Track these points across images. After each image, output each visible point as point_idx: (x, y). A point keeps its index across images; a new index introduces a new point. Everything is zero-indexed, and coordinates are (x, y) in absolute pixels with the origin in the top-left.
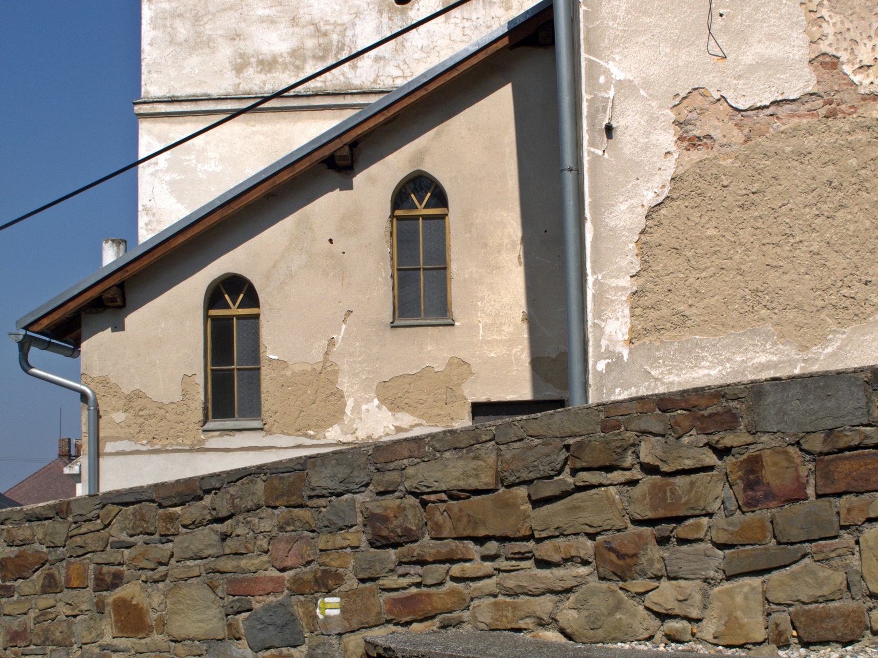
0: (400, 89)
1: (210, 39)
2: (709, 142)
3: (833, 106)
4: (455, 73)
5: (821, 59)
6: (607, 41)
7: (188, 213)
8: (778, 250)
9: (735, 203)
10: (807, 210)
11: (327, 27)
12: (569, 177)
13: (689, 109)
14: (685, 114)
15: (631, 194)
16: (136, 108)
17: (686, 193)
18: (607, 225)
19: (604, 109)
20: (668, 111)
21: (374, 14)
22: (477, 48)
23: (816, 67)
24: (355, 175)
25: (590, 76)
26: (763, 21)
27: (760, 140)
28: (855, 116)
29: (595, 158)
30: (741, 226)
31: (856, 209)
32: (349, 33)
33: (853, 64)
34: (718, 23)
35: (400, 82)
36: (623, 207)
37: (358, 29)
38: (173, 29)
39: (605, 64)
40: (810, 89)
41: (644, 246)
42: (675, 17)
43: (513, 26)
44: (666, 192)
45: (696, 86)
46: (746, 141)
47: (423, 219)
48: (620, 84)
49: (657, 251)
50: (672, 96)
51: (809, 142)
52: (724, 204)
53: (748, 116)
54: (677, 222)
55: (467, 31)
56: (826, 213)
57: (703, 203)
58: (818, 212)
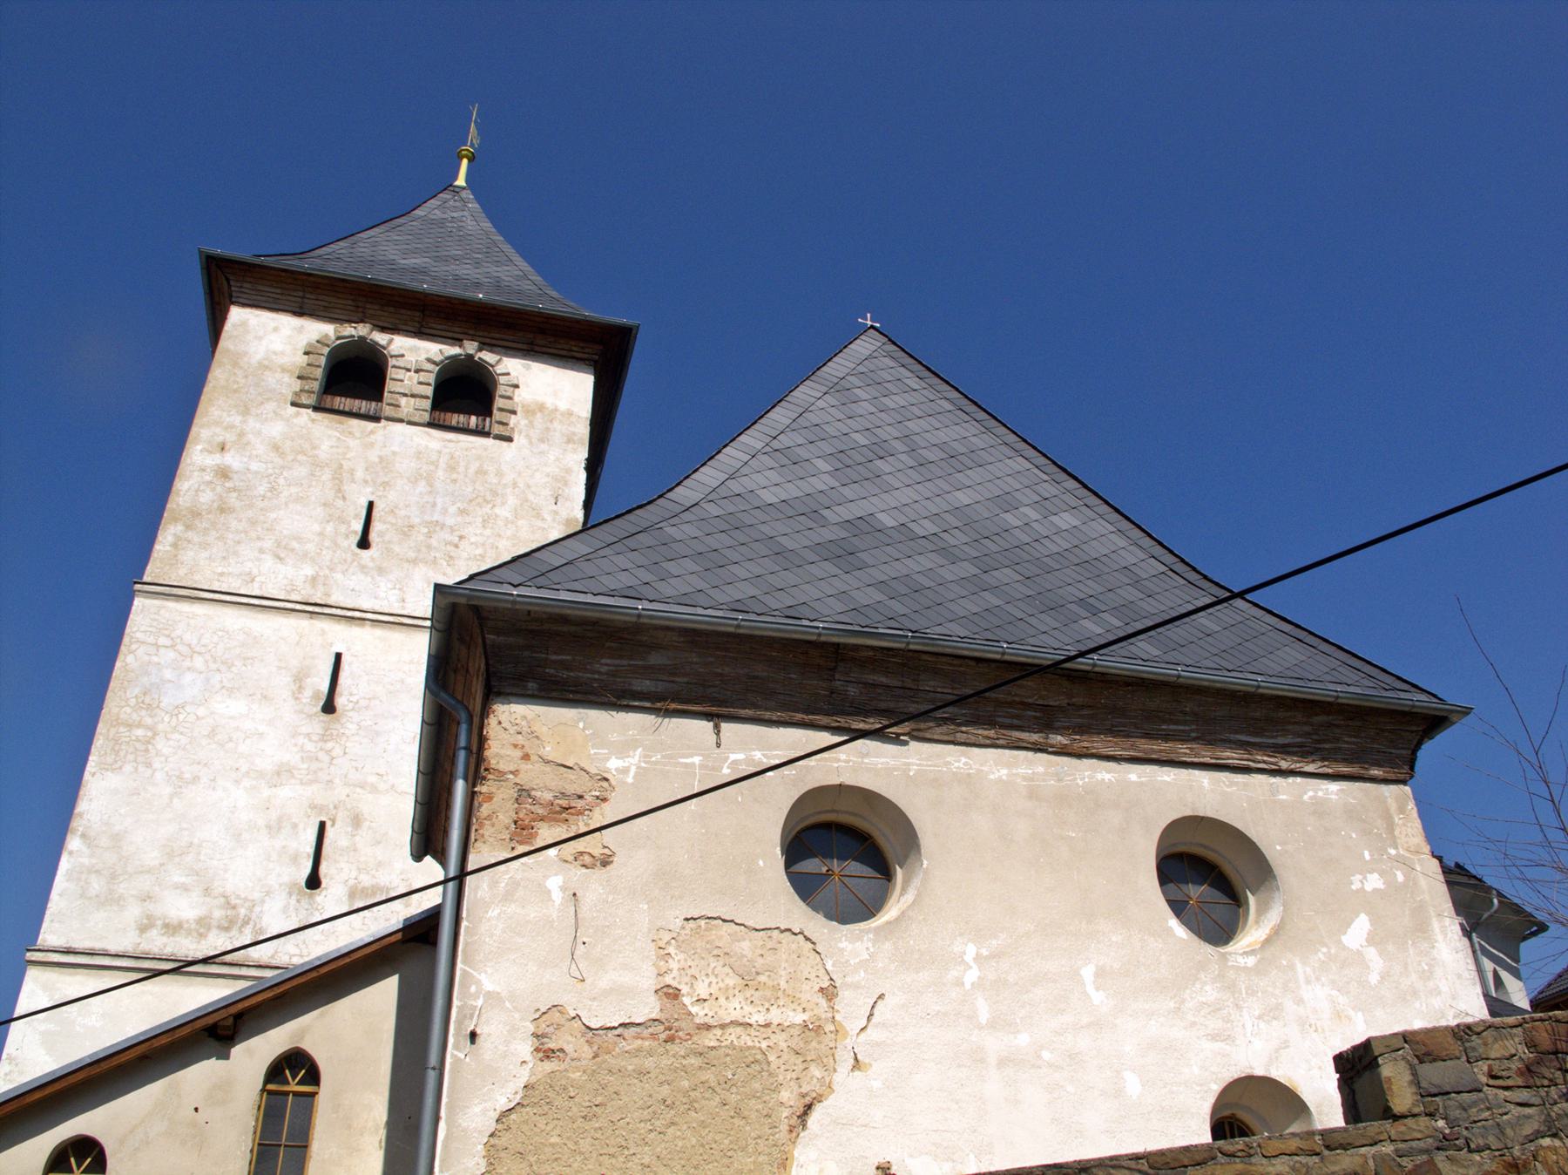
0: (296, 967)
1: (121, 898)
2: (561, 1055)
3: (673, 1032)
4: (347, 960)
5: (665, 990)
6: (482, 955)
7: (55, 1067)
8: (614, 1161)
9: (579, 1114)
10: (642, 1125)
11: (238, 901)
12: (432, 1076)
13: (547, 1023)
14: (543, 1028)
15: (486, 1098)
16: (28, 954)
17: (535, 1101)
18: (460, 1125)
19: (472, 1016)
20: (528, 1024)
21: (284, 895)
22: (372, 939)
23: (660, 996)
24: (234, 1046)
25: (462, 985)
26: (620, 952)
27: (607, 1057)
28: (690, 1042)
29: (456, 1060)
30: (582, 1136)
31: (685, 1127)
32: (257, 909)
33: (692, 997)
34: (580, 949)
35: (297, 961)
36: (477, 1109)
37: (266, 907)
38: (87, 883)
39: (478, 976)
40: (653, 1016)
41: (492, 1149)
42: (545, 941)
43: (408, 923)
44: (518, 1099)
45: (556, 1004)
46: (594, 1058)
47: (293, 1095)
48: (489, 995)
49: (503, 1154)
50: (533, 1011)
51: (649, 1063)
52: (568, 1114)
53: (598, 1035)
54: (525, 1128)
55: (366, 921)
56: (658, 1129)
57: (550, 1112)
58: (651, 1128)
